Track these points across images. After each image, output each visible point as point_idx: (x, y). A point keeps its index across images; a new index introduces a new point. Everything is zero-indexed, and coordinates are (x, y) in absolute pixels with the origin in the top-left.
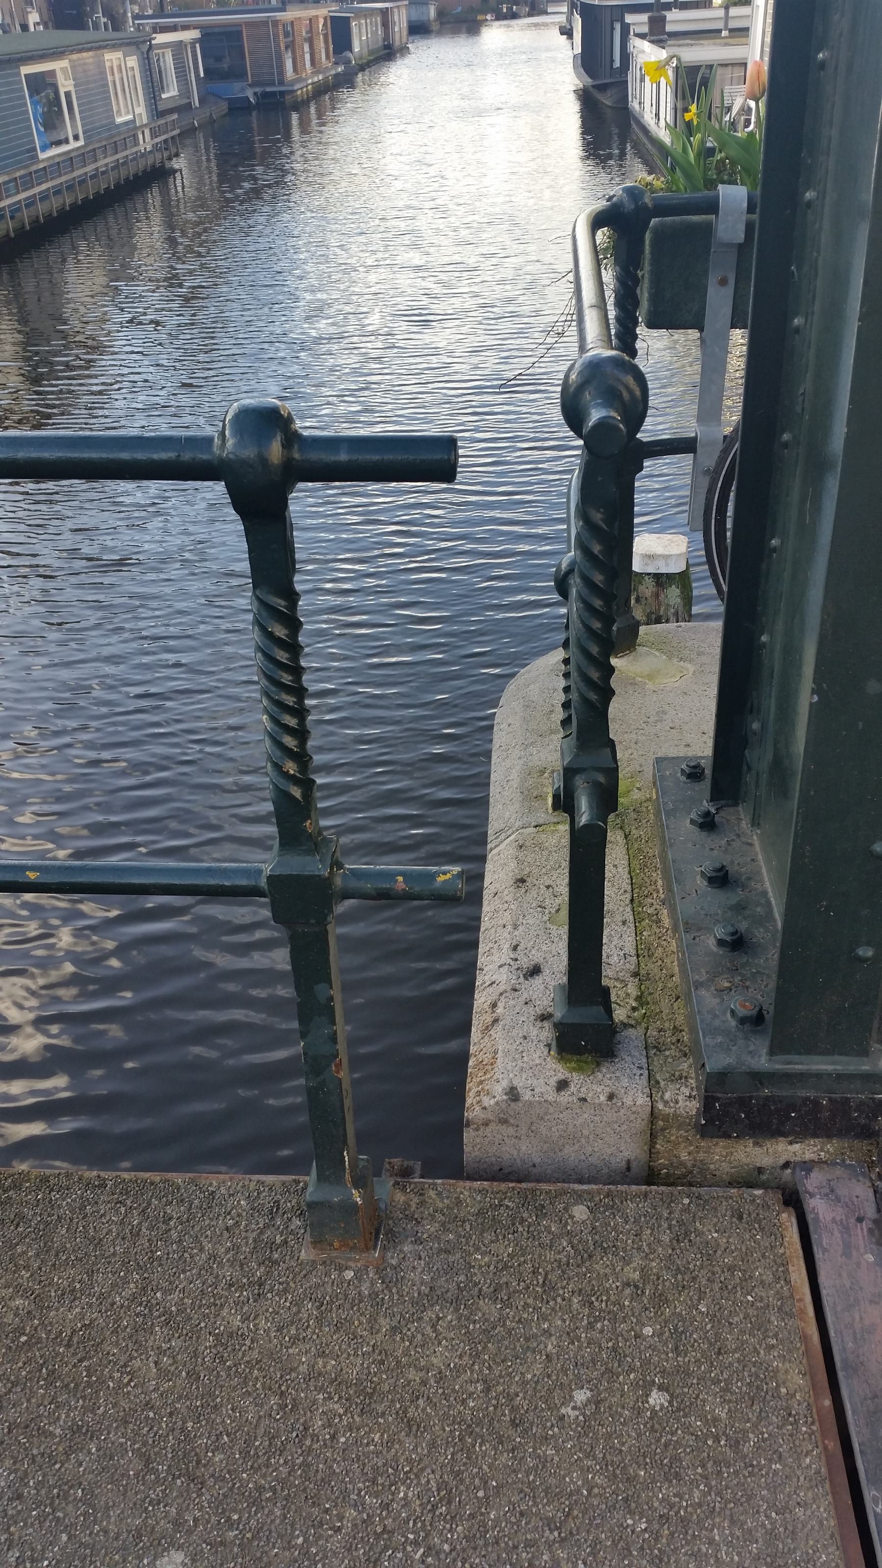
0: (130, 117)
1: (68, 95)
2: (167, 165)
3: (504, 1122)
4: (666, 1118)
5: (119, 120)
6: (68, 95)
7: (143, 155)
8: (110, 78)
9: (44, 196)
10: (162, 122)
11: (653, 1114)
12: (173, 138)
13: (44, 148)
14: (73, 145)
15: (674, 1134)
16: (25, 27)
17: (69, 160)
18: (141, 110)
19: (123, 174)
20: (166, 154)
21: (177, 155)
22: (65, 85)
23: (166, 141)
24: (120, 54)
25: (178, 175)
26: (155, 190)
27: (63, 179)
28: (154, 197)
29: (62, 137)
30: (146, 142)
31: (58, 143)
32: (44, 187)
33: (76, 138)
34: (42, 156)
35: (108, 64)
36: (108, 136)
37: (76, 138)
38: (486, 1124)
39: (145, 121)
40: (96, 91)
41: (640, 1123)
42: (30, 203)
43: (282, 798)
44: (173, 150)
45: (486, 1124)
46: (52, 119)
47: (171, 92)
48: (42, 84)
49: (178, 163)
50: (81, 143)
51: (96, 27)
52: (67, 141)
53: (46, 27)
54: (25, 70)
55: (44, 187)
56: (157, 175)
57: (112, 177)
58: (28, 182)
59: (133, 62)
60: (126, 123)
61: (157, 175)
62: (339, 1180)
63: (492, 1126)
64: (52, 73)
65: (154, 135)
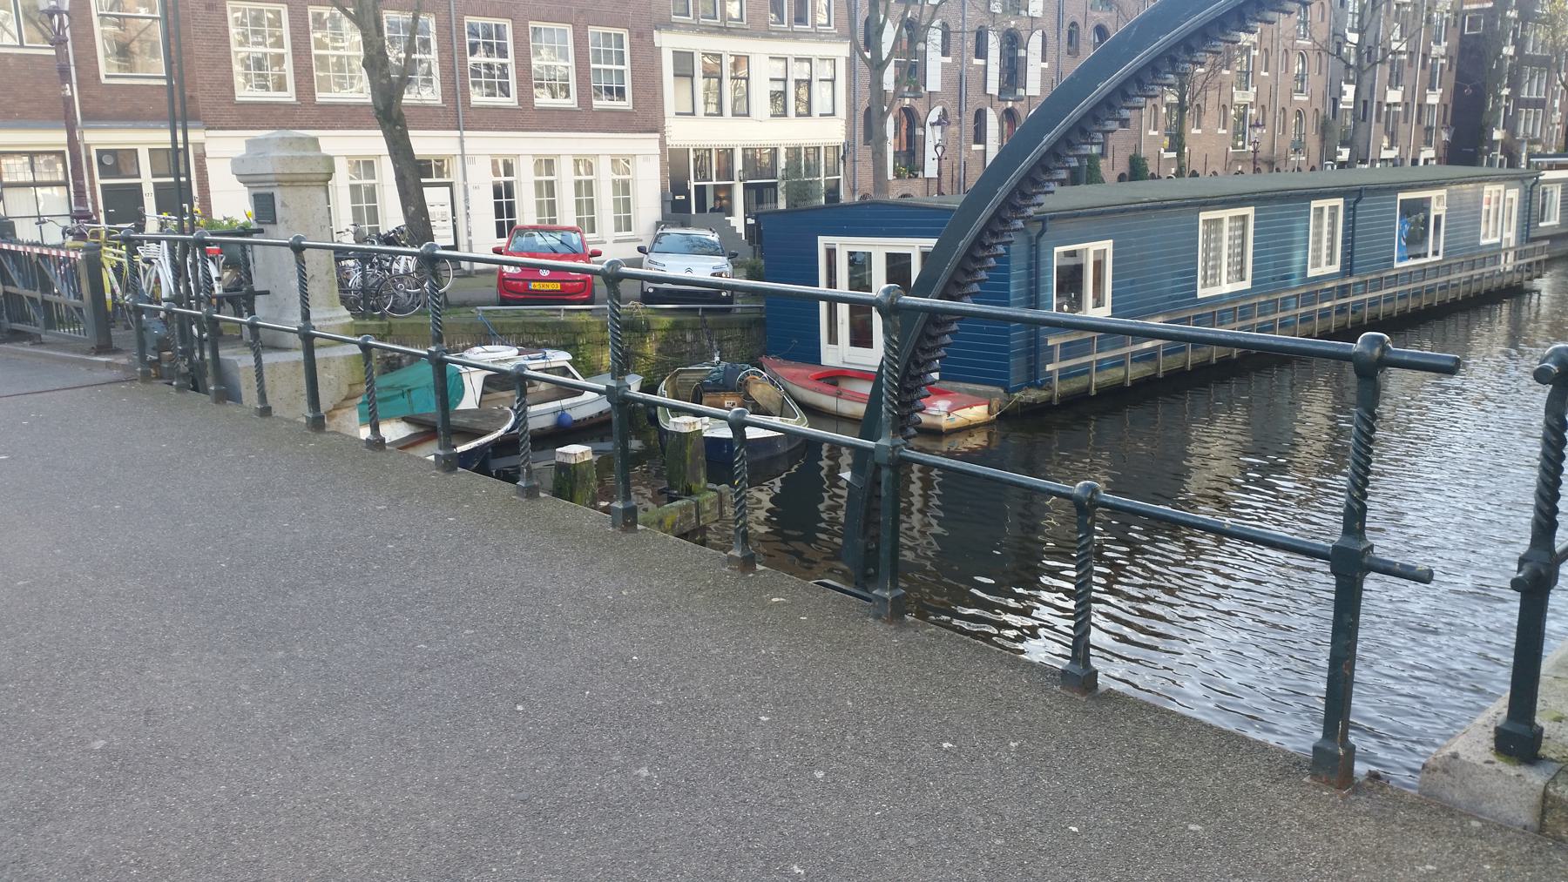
0: (1497, 240)
1: (1438, 218)
2: (1527, 285)
3: (1446, 771)
4: (1554, 799)
5: (1483, 242)
6: (1438, 218)
7: (1501, 274)
8: (1485, 207)
9: (1389, 299)
10: (1531, 246)
11: (1545, 796)
12: (1538, 263)
13: (1401, 259)
14: (1431, 258)
15: (1558, 813)
16: (1415, 162)
17: (1423, 271)
18: (1510, 236)
19: (1475, 288)
20: (1526, 275)
21: (1539, 277)
22: (1438, 209)
23: (1529, 264)
24: (1501, 187)
25: (1535, 296)
26: (1505, 307)
27: (1412, 286)
28: (1505, 310)
29: (1422, 251)
30: (1508, 263)
31: (1417, 256)
32: (1390, 291)
33: (1436, 253)
34: (1397, 265)
35: (1486, 196)
36: (1467, 252)
37: (1436, 253)
38: (1435, 770)
39: (1512, 244)
40: (1466, 217)
41: (1535, 799)
42: (1374, 302)
43: (1349, 507)
44: (1536, 273)
45: (1435, 770)
46: (1416, 240)
47: (1553, 220)
48: (1416, 209)
49: (1544, 284)
50: (1440, 257)
51: (1491, 163)
52: (1425, 255)
53: (1439, 162)
54: (1402, 196)
55: (1390, 291)
56: (1514, 292)
57: (1462, 290)
58: (1378, 284)
59: (1514, 194)
60: (1492, 245)
61: (1514, 292)
62: (1334, 740)
63: (1438, 773)
64: (1429, 199)
65: (1518, 256)
